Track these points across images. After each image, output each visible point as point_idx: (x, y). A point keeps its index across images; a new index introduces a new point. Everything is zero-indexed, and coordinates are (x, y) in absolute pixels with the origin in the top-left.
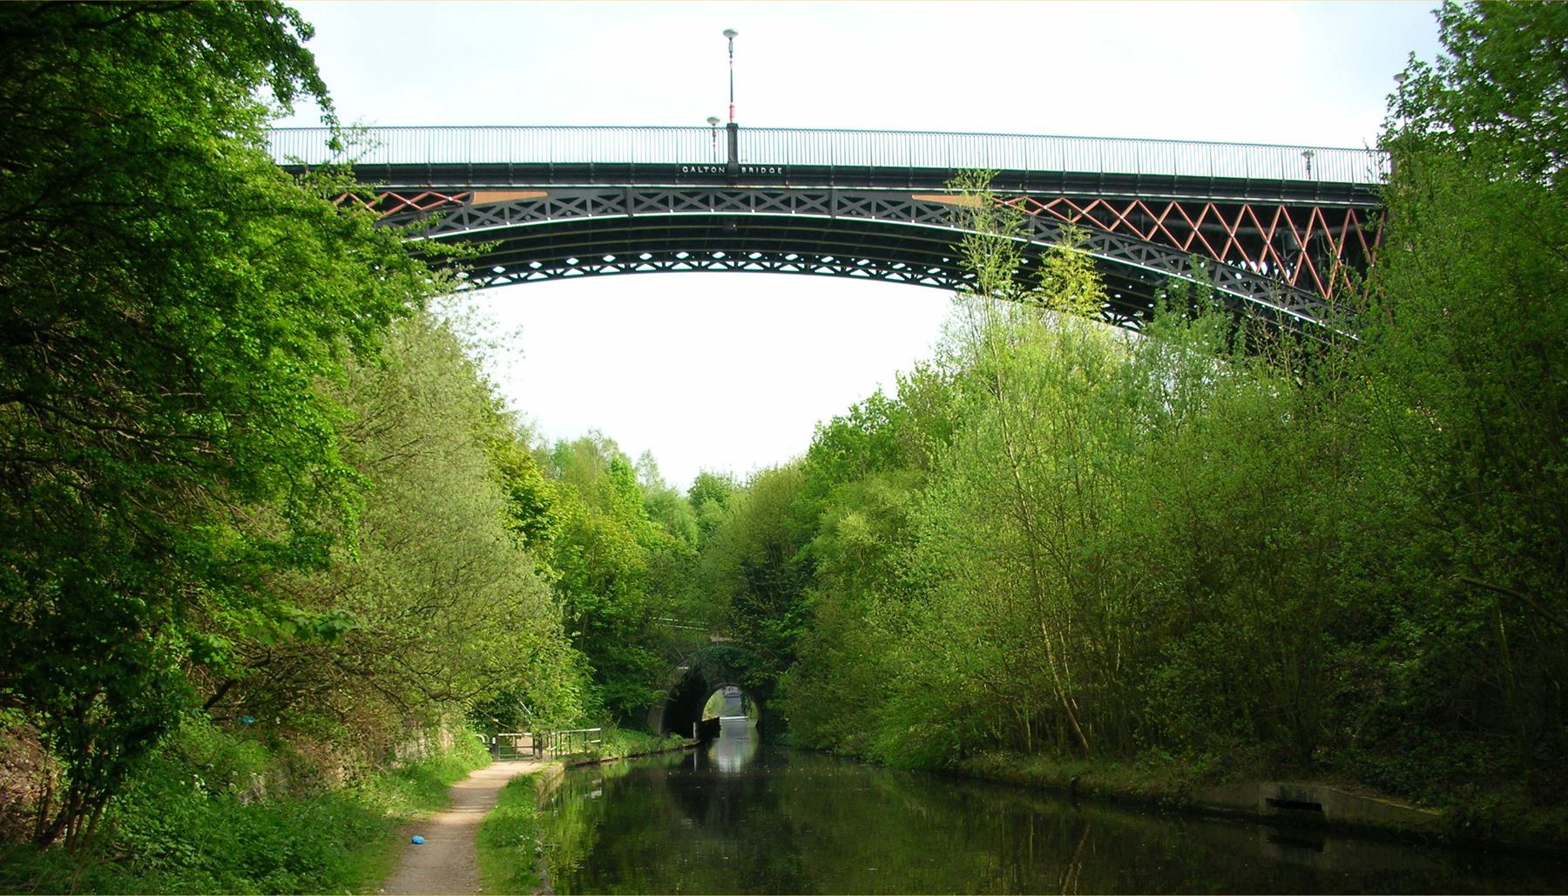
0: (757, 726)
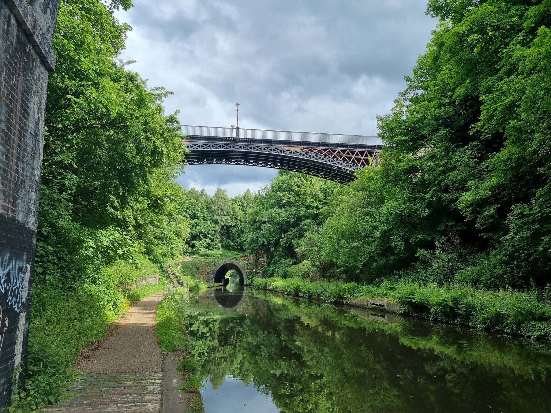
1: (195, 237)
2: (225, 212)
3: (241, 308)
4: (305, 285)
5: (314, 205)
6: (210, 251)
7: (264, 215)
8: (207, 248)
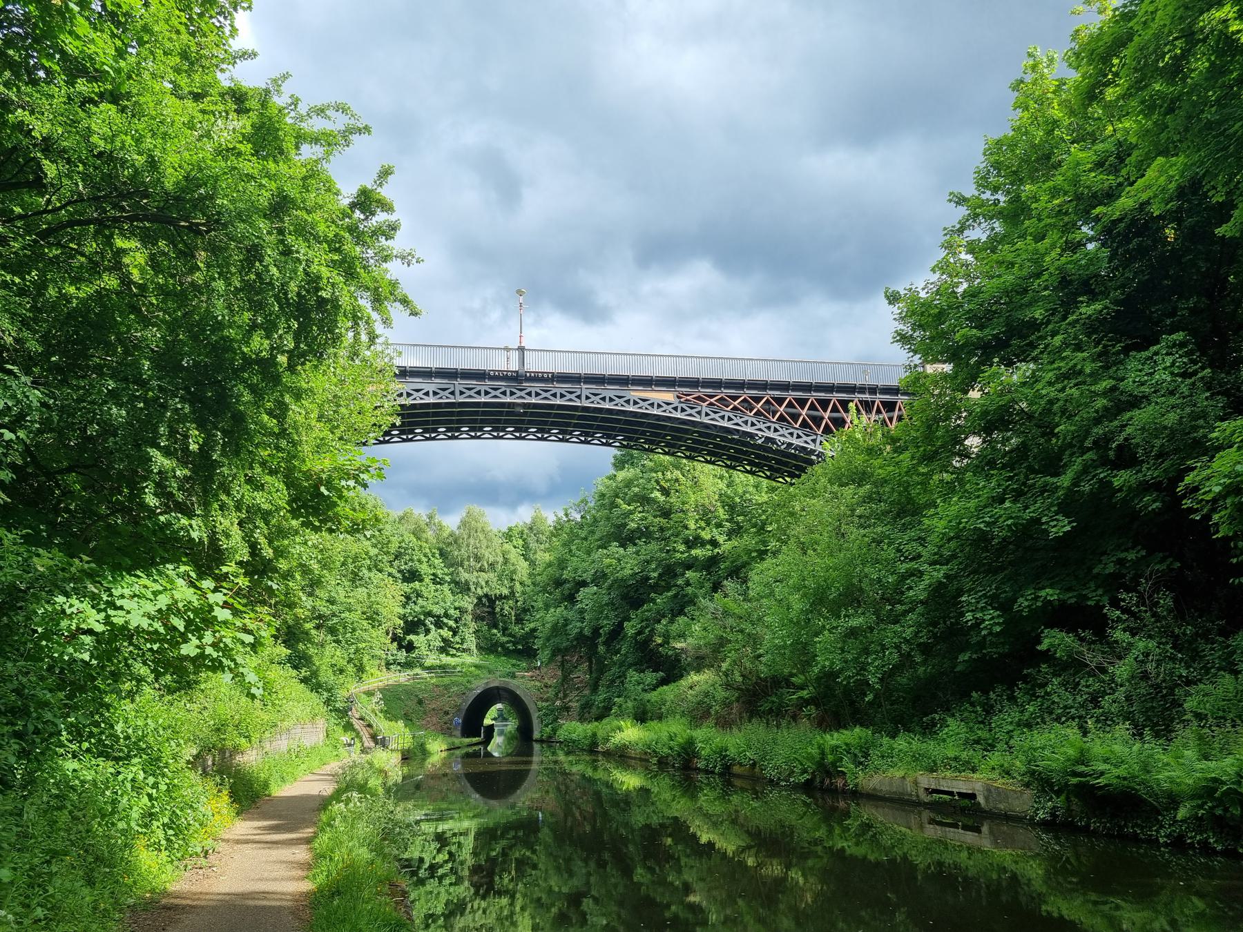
0: (483, 795)
1: (413, 626)
2: (486, 564)
3: (526, 799)
4: (708, 739)
5: (706, 535)
6: (449, 658)
7: (581, 566)
8: (443, 650)
